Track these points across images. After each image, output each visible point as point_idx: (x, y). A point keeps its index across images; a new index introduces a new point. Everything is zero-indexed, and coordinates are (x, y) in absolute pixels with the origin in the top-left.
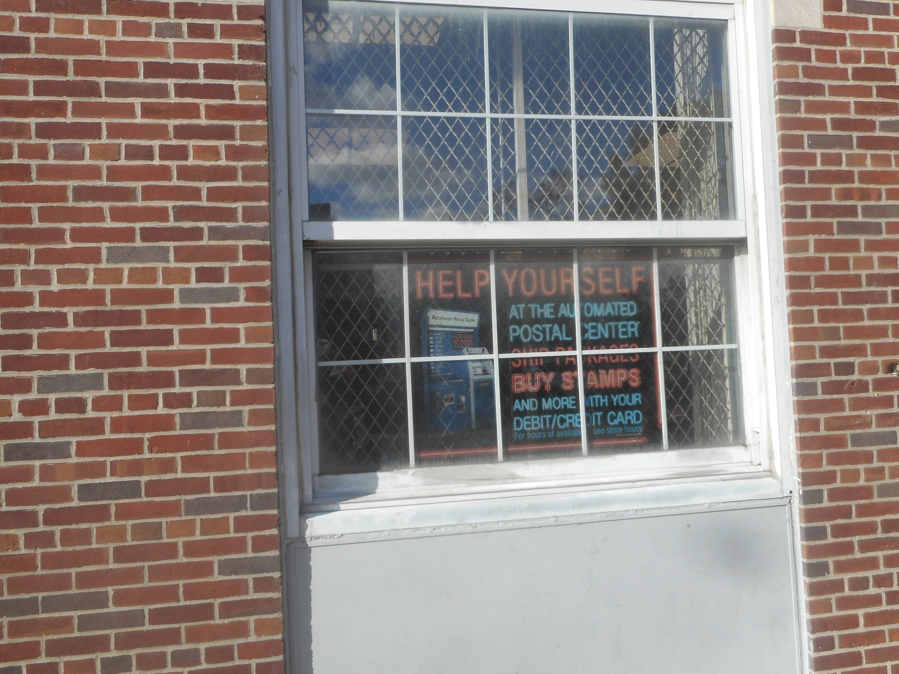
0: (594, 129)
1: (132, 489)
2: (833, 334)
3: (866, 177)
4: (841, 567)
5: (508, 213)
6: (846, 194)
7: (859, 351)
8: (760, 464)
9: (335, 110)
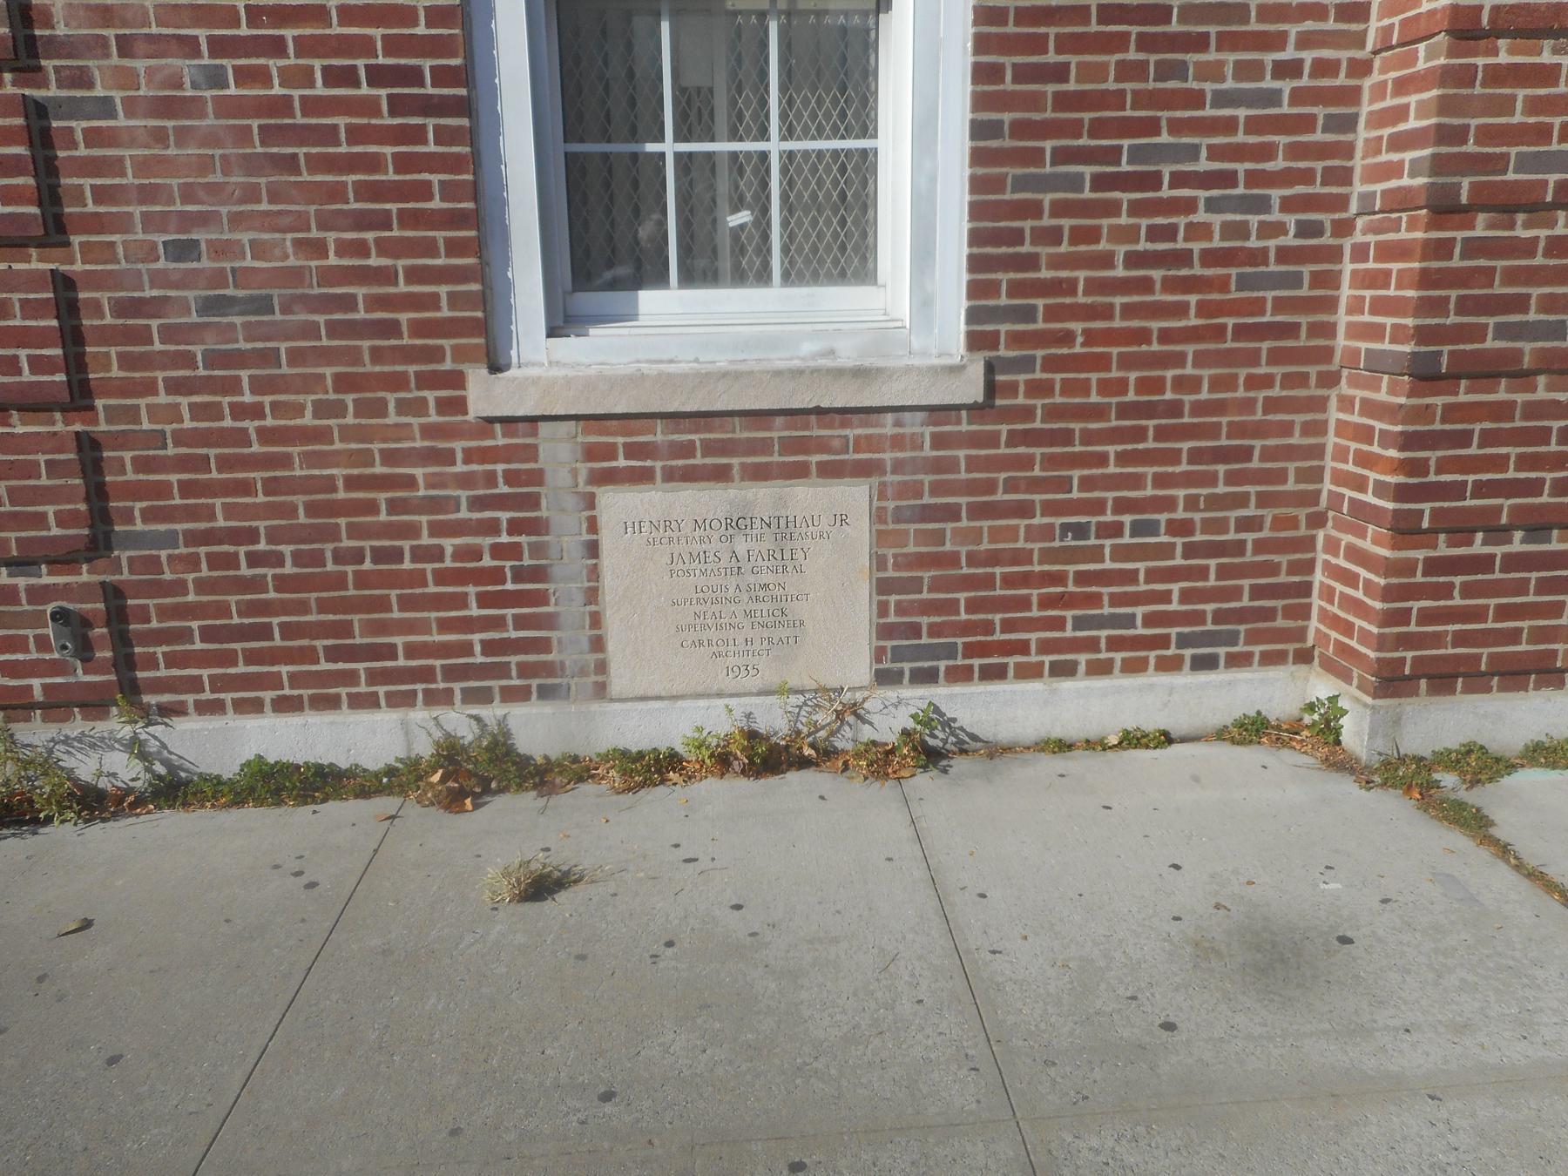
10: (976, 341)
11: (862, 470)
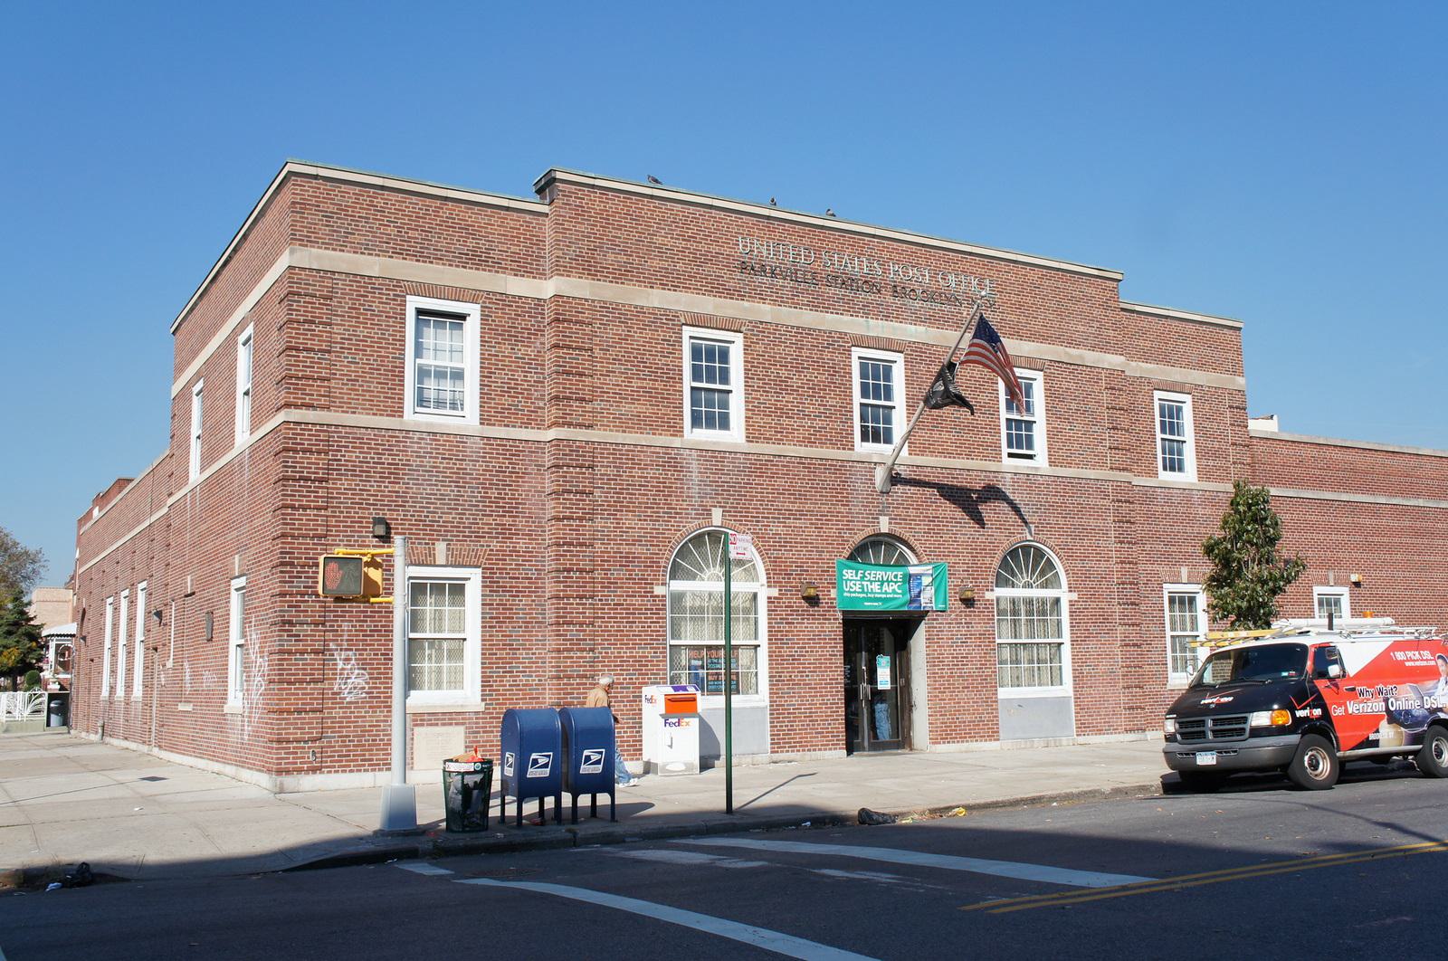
2: (778, 668)
3: (786, 631)
4: (777, 722)
6: (782, 636)
7: (783, 672)
10: (483, 700)
11: (463, 724)
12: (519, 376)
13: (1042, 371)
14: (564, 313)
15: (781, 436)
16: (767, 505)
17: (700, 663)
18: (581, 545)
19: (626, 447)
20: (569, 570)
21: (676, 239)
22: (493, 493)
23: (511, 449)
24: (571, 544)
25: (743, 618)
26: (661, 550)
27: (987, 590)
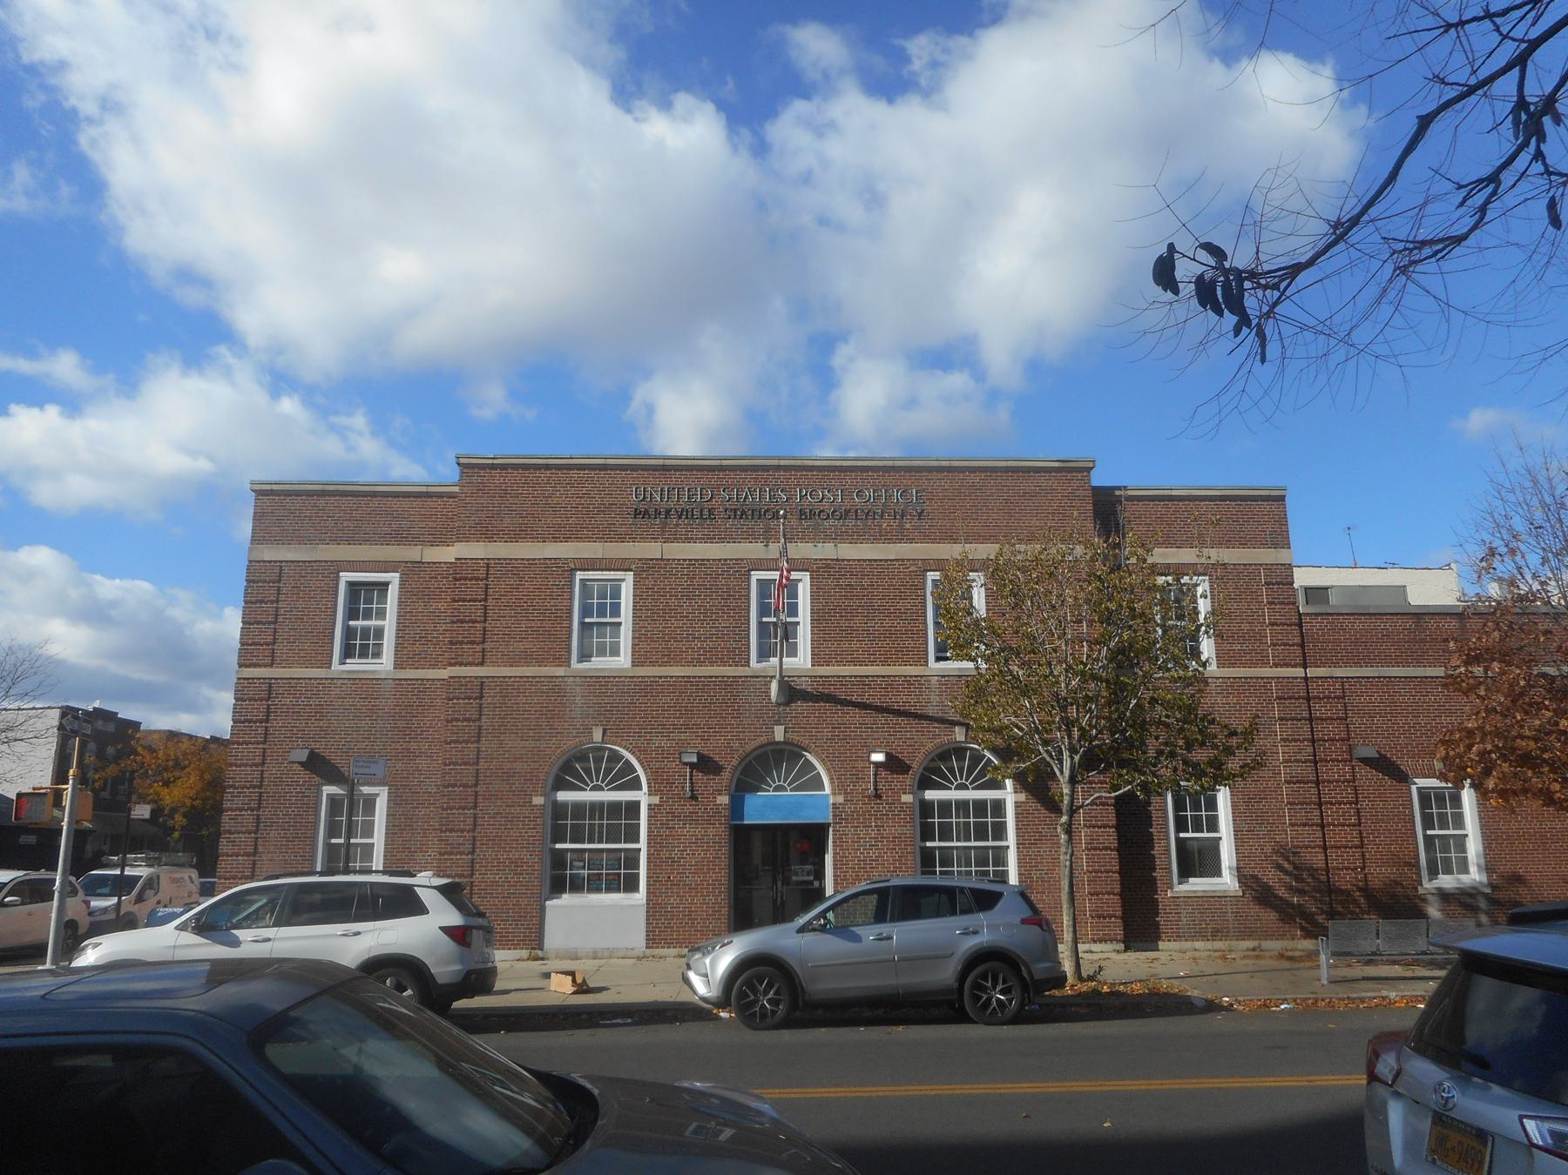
0: (1197, 821)
1: (516, 893)
5: (600, 841)
8: (374, 775)
9: (927, 792)
12: (430, 627)
13: (807, 571)
14: (459, 572)
15: (670, 658)
16: (651, 721)
17: (582, 864)
18: (465, 764)
19: (512, 679)
20: (454, 786)
21: (571, 497)
22: (401, 724)
23: (422, 685)
24: (455, 764)
25: (603, 824)
26: (541, 765)
27: (904, 793)
